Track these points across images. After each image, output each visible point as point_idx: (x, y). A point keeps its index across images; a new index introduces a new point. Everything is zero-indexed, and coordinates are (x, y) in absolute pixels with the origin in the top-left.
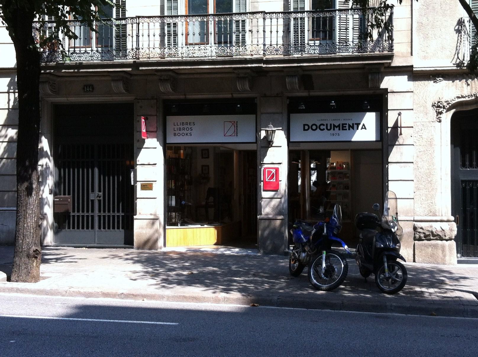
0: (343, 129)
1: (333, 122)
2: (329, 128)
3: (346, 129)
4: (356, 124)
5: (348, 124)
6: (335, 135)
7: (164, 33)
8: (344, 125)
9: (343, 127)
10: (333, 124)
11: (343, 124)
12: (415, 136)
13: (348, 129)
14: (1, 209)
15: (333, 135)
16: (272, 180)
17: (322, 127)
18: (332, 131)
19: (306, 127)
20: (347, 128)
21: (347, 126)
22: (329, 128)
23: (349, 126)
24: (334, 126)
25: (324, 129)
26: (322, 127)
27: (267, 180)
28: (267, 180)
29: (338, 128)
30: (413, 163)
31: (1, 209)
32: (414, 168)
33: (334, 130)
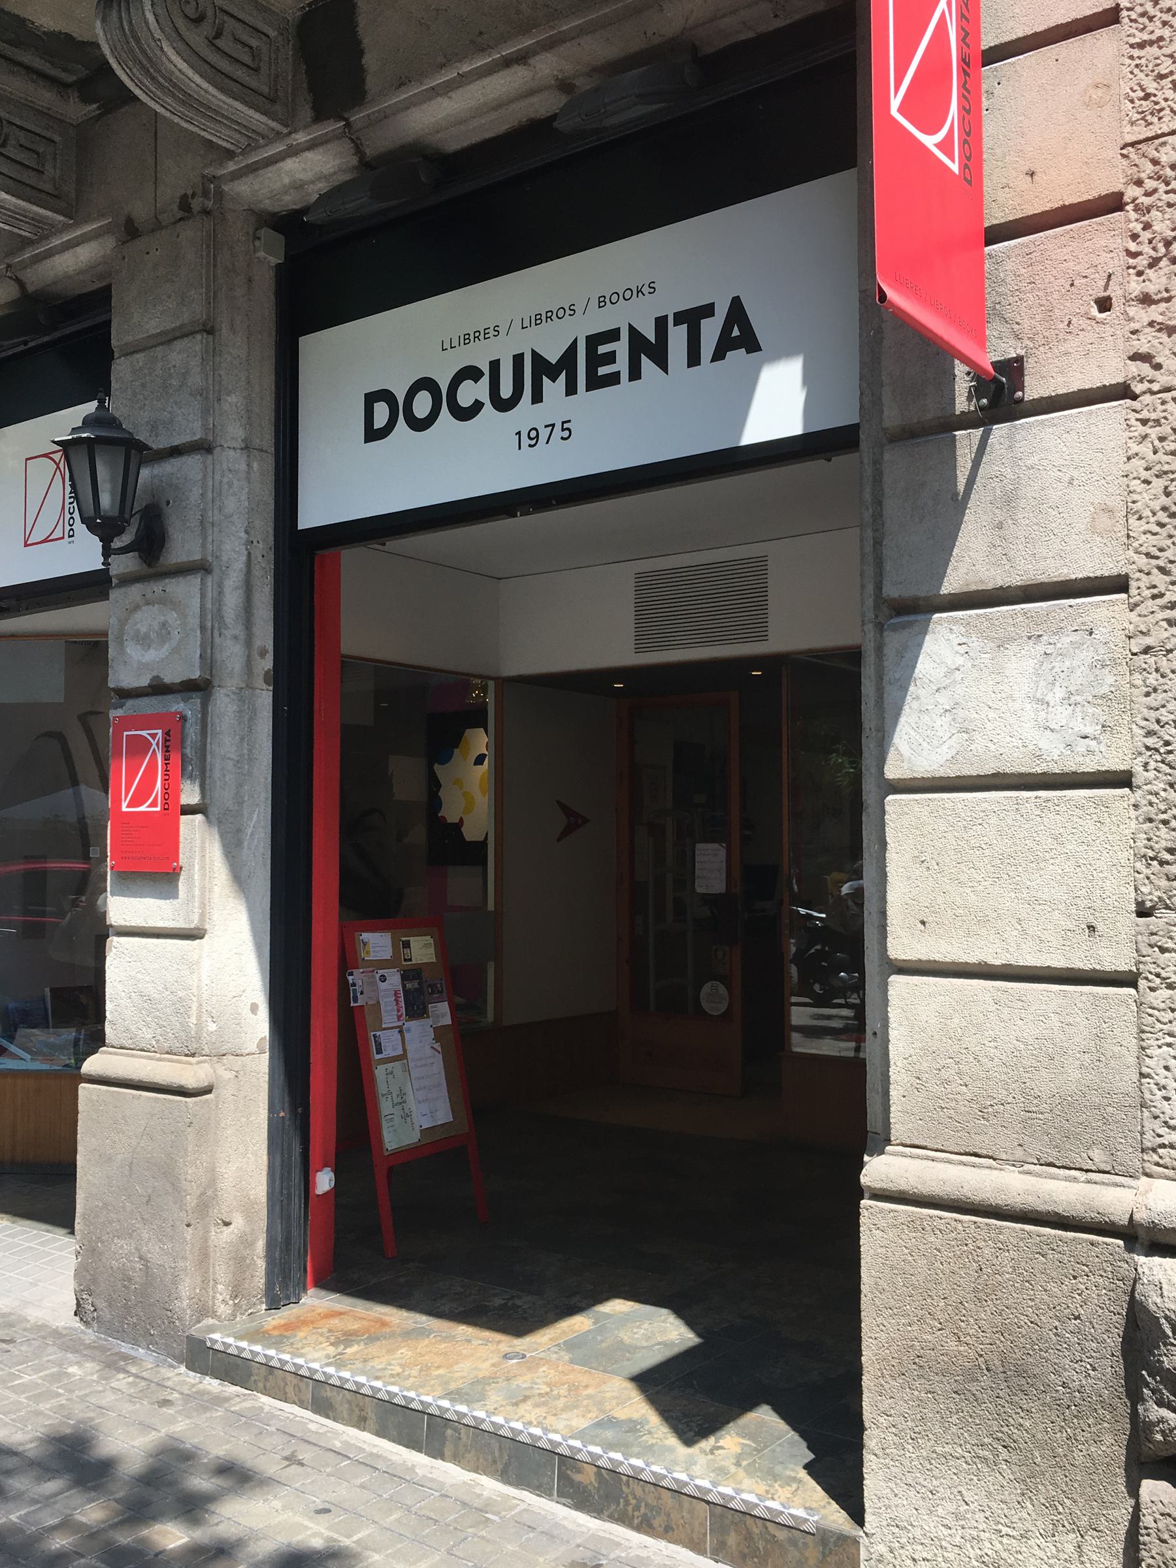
0: (595, 383)
1: (526, 342)
2: (506, 391)
3: (614, 379)
4: (680, 318)
5: (625, 335)
6: (544, 433)
7: (219, 615)
8: (602, 349)
9: (594, 360)
10: (535, 354)
11: (594, 341)
12: (1136, 287)
13: (624, 376)
14: (9, 51)
15: (534, 437)
16: (143, 808)
17: (468, 394)
18: (526, 413)
19: (381, 412)
20: (622, 365)
21: (621, 348)
22: (506, 391)
23: (638, 343)
24: (541, 367)
25: (477, 406)
26: (468, 394)
27: (124, 809)
28: (124, 809)
29: (562, 377)
30: (1118, 584)
31: (9, 51)
32: (1136, 645)
33: (537, 397)
